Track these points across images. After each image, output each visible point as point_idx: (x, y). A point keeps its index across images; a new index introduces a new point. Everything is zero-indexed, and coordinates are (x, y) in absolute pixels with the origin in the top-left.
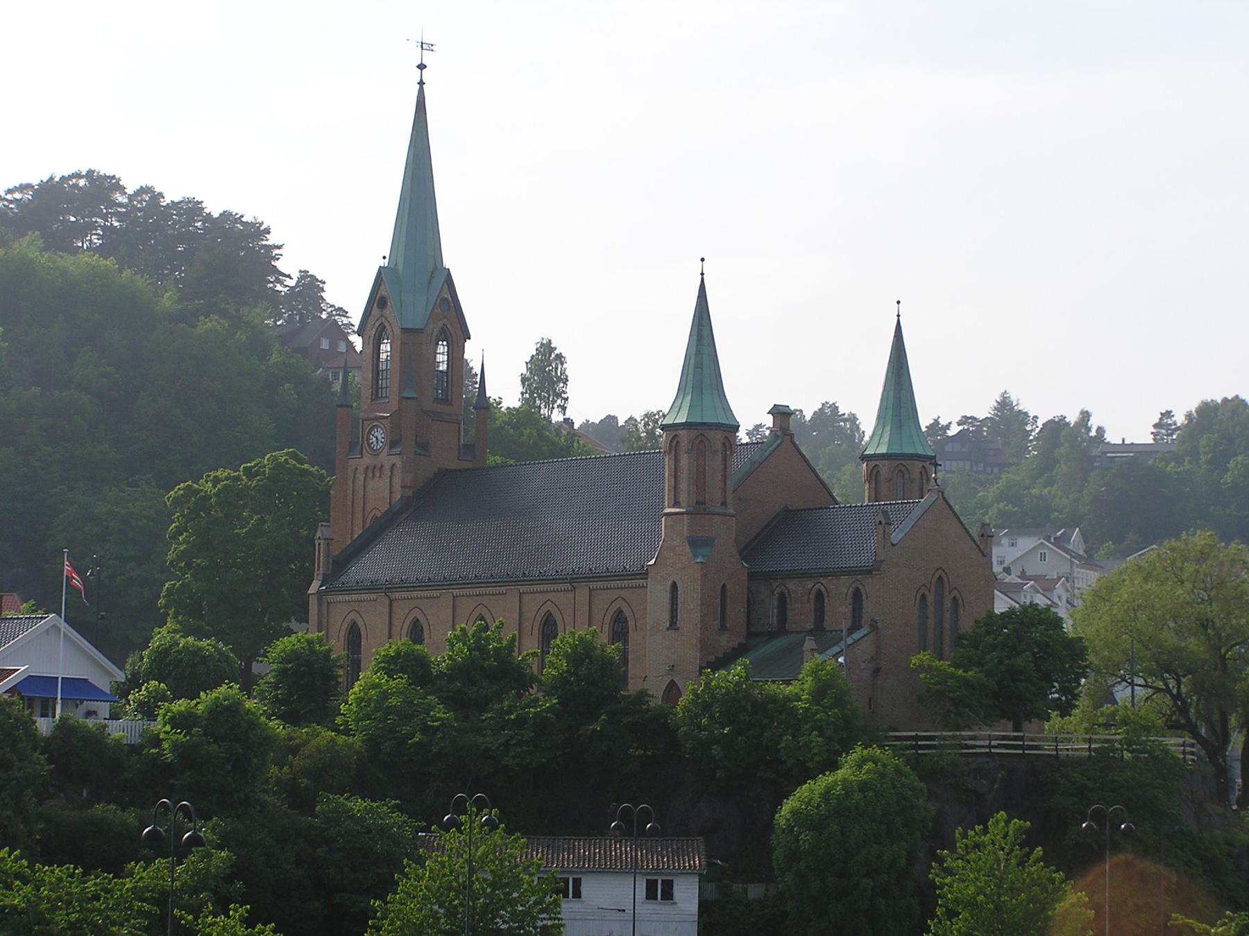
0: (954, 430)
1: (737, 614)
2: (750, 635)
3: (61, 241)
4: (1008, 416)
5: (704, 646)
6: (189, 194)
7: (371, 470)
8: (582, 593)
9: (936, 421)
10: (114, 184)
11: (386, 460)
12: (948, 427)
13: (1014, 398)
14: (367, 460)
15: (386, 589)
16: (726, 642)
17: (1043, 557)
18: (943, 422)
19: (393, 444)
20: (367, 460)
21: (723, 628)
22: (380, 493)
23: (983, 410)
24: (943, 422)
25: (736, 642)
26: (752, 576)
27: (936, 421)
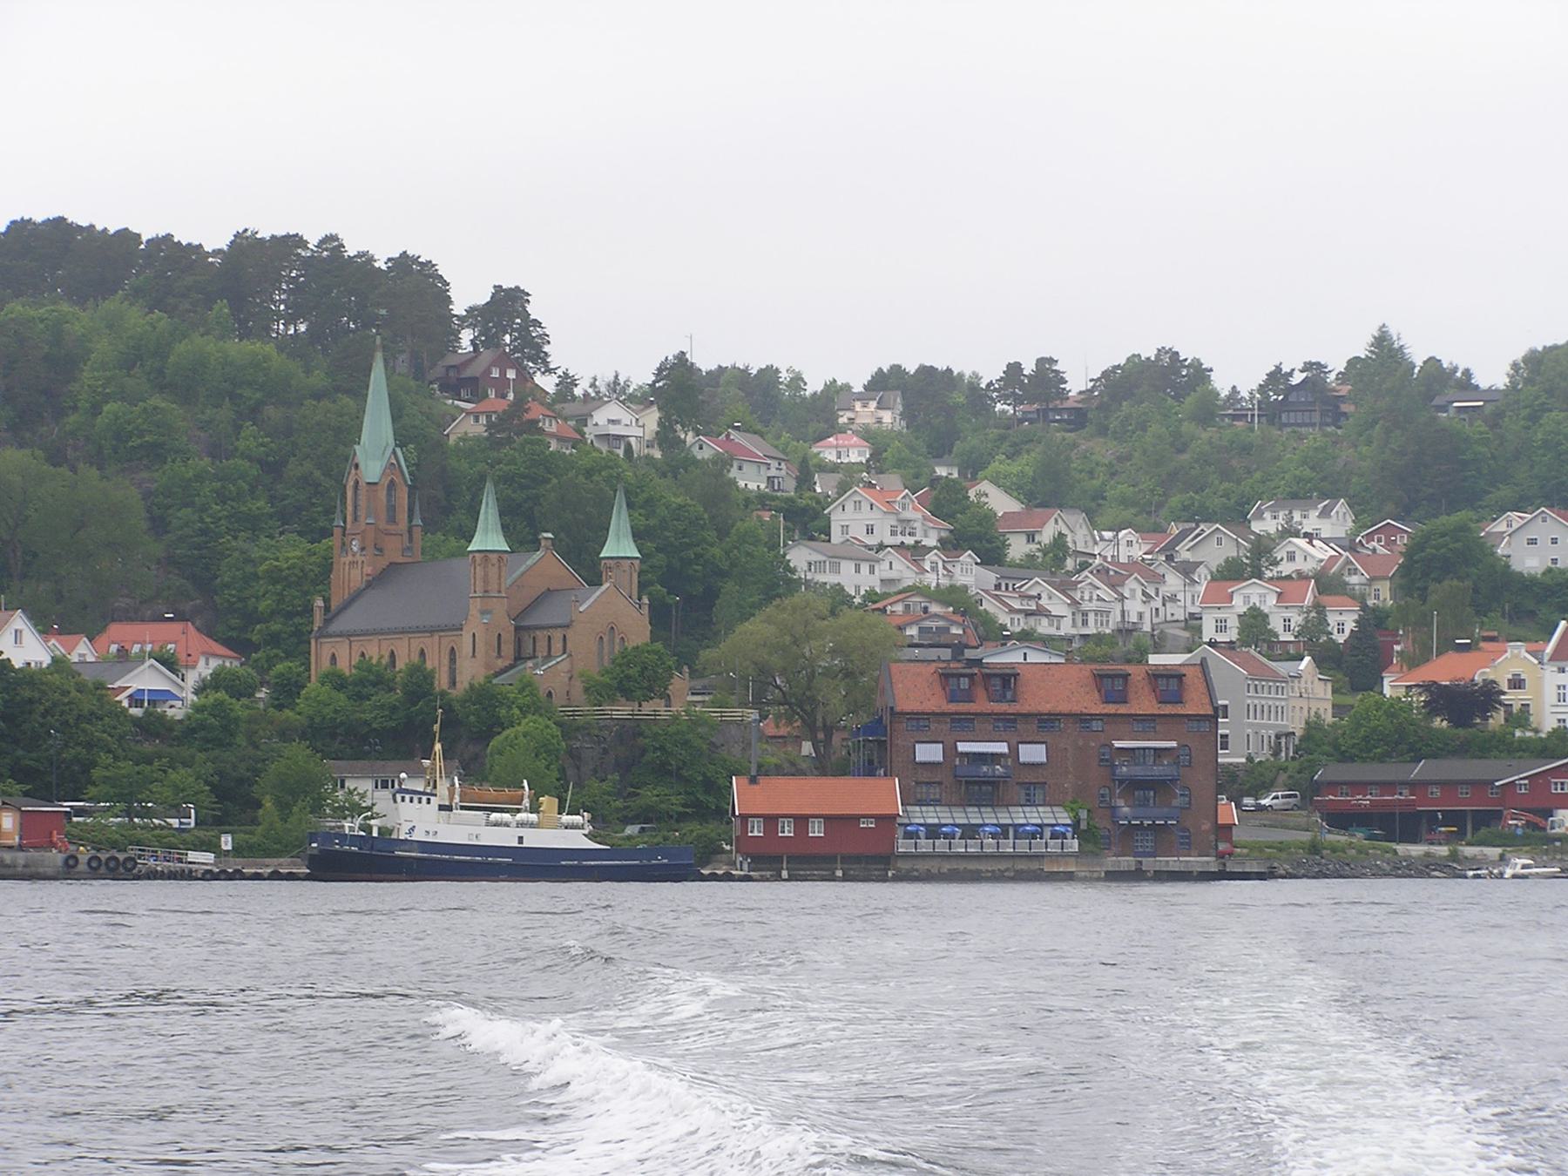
0: (1297, 378)
1: (508, 649)
2: (516, 659)
3: (250, 322)
4: (1277, 377)
5: (488, 666)
6: (363, 249)
7: (352, 563)
8: (436, 637)
9: (1278, 369)
10: (297, 241)
11: (359, 558)
12: (1291, 374)
13: (1393, 331)
14: (350, 558)
15: (348, 635)
16: (501, 664)
17: (1219, 542)
18: (1286, 369)
19: (363, 549)
20: (350, 558)
21: (499, 656)
22: (356, 578)
23: (1361, 348)
24: (1286, 369)
25: (507, 663)
26: (517, 629)
27: (1278, 369)
